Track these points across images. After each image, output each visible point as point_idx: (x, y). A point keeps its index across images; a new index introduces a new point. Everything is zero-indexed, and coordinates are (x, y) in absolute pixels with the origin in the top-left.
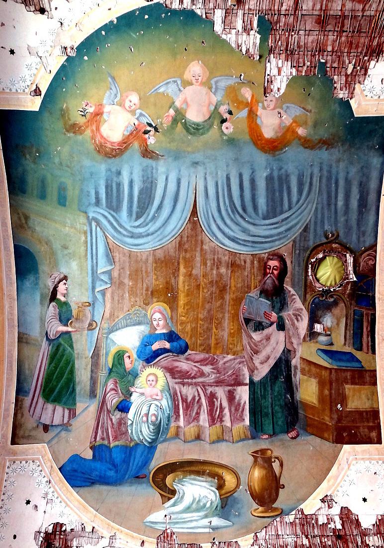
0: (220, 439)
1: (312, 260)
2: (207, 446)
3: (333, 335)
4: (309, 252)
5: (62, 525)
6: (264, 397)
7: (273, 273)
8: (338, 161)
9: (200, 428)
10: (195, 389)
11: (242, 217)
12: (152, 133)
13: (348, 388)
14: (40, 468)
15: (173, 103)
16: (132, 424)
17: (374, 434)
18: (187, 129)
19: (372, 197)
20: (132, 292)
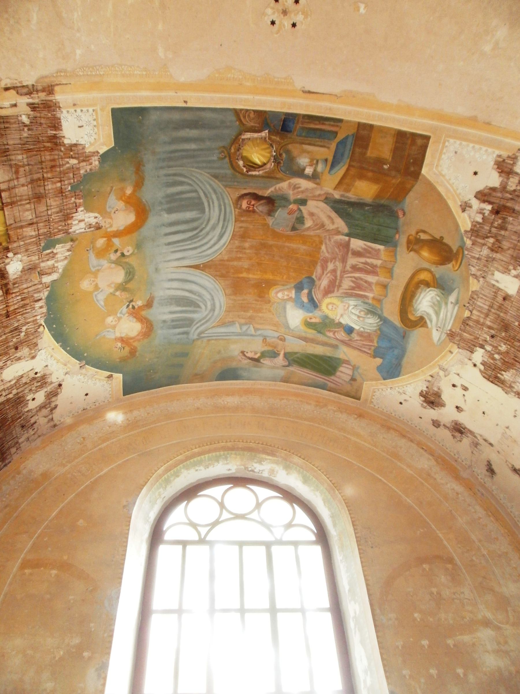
0: (390, 272)
1: (245, 170)
2: (394, 282)
3: (318, 157)
4: (237, 174)
5: (422, 391)
6: (363, 228)
7: (253, 205)
8: (154, 153)
9: (378, 284)
10: (346, 279)
11: (201, 231)
12: (133, 303)
13: (371, 153)
14: (380, 390)
15: (111, 293)
16: (363, 328)
17: (419, 142)
18: (131, 280)
19: (187, 116)
20: (259, 311)
